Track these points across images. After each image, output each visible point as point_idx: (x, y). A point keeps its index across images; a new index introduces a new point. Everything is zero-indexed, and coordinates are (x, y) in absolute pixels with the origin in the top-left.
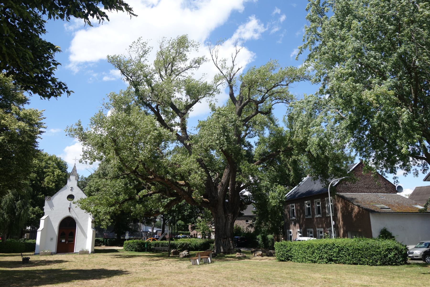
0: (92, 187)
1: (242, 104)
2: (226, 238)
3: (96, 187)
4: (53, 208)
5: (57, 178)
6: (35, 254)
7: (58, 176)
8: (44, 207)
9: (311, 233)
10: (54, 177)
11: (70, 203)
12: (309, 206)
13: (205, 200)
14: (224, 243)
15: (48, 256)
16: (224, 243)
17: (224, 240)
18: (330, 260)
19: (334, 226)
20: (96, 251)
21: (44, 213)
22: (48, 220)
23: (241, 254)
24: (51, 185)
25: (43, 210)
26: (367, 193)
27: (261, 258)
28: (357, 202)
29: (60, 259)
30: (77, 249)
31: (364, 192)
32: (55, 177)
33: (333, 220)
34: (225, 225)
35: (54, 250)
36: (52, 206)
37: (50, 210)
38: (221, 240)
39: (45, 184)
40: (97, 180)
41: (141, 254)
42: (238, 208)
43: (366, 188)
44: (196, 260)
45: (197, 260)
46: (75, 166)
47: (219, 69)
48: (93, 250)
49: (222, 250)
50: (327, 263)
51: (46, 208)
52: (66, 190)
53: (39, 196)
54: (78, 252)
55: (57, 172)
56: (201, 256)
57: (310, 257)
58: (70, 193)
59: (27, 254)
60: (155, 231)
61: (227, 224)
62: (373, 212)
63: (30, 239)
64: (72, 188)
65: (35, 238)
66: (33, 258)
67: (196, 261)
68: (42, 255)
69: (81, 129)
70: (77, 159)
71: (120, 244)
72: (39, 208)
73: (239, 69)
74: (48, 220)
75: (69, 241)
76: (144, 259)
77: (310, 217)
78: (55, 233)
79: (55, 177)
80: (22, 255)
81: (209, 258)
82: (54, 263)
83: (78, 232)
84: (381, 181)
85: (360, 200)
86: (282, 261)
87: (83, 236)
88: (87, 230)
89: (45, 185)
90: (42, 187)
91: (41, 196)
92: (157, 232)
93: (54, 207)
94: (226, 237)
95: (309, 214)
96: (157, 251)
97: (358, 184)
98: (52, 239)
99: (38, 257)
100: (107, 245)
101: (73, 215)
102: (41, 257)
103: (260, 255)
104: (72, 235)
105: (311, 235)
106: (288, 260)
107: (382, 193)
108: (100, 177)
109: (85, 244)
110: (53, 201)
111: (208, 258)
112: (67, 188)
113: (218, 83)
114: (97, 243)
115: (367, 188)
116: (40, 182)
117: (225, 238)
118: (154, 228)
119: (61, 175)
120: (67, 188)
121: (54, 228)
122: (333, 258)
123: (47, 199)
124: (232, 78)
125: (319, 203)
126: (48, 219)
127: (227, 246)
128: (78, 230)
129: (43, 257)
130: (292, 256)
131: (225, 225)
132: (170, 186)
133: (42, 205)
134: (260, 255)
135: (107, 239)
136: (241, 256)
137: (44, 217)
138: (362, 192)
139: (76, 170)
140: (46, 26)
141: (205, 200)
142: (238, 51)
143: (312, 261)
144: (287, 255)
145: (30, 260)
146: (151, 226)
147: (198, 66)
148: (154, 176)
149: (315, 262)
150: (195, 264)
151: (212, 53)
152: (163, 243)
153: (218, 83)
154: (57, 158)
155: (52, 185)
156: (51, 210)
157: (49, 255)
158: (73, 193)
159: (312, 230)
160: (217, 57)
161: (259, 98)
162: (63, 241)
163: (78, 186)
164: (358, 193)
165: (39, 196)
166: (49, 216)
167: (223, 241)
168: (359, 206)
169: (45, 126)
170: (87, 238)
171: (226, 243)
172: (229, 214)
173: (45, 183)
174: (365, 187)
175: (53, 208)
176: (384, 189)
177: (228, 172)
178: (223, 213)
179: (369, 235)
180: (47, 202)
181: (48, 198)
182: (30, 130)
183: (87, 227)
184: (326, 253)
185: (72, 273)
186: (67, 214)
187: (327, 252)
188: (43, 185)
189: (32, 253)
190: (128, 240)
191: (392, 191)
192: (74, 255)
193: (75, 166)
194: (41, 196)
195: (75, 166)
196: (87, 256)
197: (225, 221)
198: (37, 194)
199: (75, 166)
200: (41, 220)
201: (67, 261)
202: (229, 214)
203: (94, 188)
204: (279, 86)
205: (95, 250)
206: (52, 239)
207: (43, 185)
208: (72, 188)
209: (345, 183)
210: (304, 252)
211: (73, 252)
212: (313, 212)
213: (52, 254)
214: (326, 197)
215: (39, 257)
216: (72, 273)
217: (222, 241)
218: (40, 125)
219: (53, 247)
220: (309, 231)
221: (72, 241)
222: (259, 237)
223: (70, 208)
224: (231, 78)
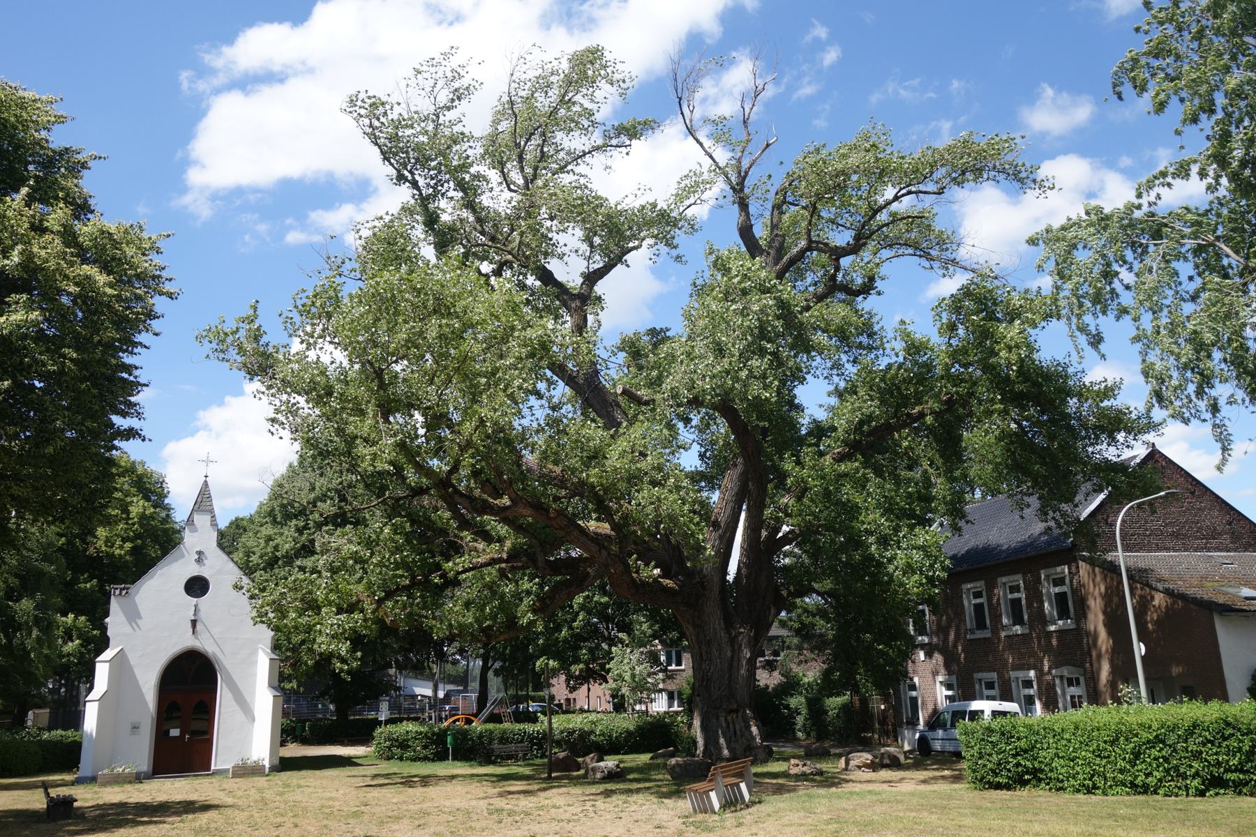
0: (254, 554)
1: (785, 260)
2: (736, 711)
3: (266, 554)
4: (139, 622)
5: (141, 525)
6: (78, 782)
7: (143, 517)
8: (107, 620)
9: (990, 686)
10: (127, 524)
11: (196, 606)
12: (978, 601)
13: (667, 582)
14: (728, 725)
15: (128, 787)
16: (728, 725)
17: (729, 718)
18: (1215, 783)
19: (1143, 658)
20: (285, 765)
21: (108, 639)
22: (121, 666)
23: (804, 765)
24: (121, 547)
25: (104, 628)
26: (1176, 551)
27: (869, 775)
28: (1159, 580)
29: (162, 798)
30: (222, 758)
31: (1168, 549)
32: (134, 524)
33: (1140, 640)
34: (731, 666)
35: (144, 764)
36: (133, 616)
37: (127, 629)
38: (718, 718)
39: (97, 545)
40: (268, 530)
41: (441, 769)
42: (769, 609)
43: (1172, 534)
44: (707, 793)
45: (713, 795)
46: (206, 484)
47: (701, 144)
48: (277, 762)
49: (726, 752)
50: (1202, 794)
51: (116, 622)
52: (181, 561)
53: (82, 586)
54: (227, 770)
55: (138, 507)
56: (724, 777)
57: (1121, 771)
58: (193, 570)
59: (62, 785)
60: (441, 694)
61: (735, 664)
62: (1226, 610)
63: (50, 729)
64: (200, 553)
65: (75, 720)
66: (86, 797)
67: (709, 798)
68: (104, 784)
69: (256, 336)
70: (204, 464)
71: (362, 734)
72: (88, 620)
73: (768, 145)
74: (121, 666)
75: (194, 733)
76: (478, 789)
77: (987, 634)
78: (145, 703)
79: (134, 524)
80: (45, 786)
81: (743, 786)
82: (178, 813)
83: (224, 698)
84: (1216, 513)
85: (1165, 573)
86: (998, 786)
87: (240, 716)
88: (253, 694)
89: (98, 551)
90: (90, 557)
91: (88, 586)
92: (448, 695)
93: (140, 618)
94: (735, 706)
95: (981, 625)
96: (488, 760)
97: (1146, 522)
98: (135, 728)
99: (96, 793)
100: (305, 741)
101: (206, 645)
102: (103, 789)
103: (867, 766)
104: (206, 709)
105: (987, 692)
106: (1024, 783)
107: (1221, 550)
108: (275, 522)
109: (247, 740)
110: (137, 599)
111: (737, 785)
112: (183, 556)
113: (687, 202)
114: (288, 732)
115: (1175, 535)
116: (84, 541)
117: (732, 711)
118: (441, 686)
119: (152, 517)
120: (183, 556)
121: (144, 691)
122: (1229, 776)
123: (117, 592)
124: (747, 173)
125: (978, 595)
126: (120, 663)
127: (742, 736)
128: (223, 696)
129: (109, 789)
130: (1042, 771)
131: (731, 666)
132: (563, 533)
133: (97, 611)
134: (867, 766)
135: (304, 721)
136: (807, 769)
137: (108, 654)
138: (1159, 549)
139: (210, 497)
140: (50, 139)
141: (667, 582)
142: (760, 87)
143: (1133, 785)
144: (1018, 765)
145: (76, 804)
146: (431, 677)
147: (628, 142)
148: (511, 499)
149: (1145, 789)
150: (707, 809)
151: (679, 91)
152: (505, 732)
153: (687, 202)
154: (134, 462)
155: (121, 550)
156: (131, 630)
157: (130, 782)
158: (205, 572)
159: (994, 676)
160: (691, 108)
161: (841, 238)
162: (175, 732)
163: (221, 546)
164: (1149, 551)
165: (82, 586)
166: (125, 650)
167: (726, 719)
168: (1168, 592)
169: (168, 287)
170: (254, 720)
171: (737, 728)
172: (742, 630)
173: (100, 543)
174: (1167, 532)
175: (139, 622)
176: (1226, 540)
177: (736, 489)
178: (723, 626)
179: (1214, 688)
180: (118, 603)
181: (121, 590)
182: (119, 298)
183: (254, 685)
184: (1197, 755)
185: (146, 819)
186: (184, 641)
187: (1201, 752)
188: (91, 550)
189: (68, 777)
190: (388, 722)
191: (1250, 545)
192: (214, 780)
193: (206, 484)
194: (88, 586)
195: (206, 481)
196: (261, 781)
197: (729, 654)
198: (75, 581)
199: (206, 481)
200: (97, 665)
201: (206, 808)
202: (742, 630)
203: (261, 557)
204: (914, 196)
205: (282, 759)
206: (135, 728)
207: (91, 550)
208: (200, 553)
209: (1106, 521)
210: (1099, 756)
211: (209, 769)
212: (997, 618)
213: (138, 778)
214: (1045, 567)
215: (96, 789)
216: (146, 819)
217: (722, 719)
218: (152, 281)
219: (141, 753)
220: (980, 680)
221: (205, 733)
222: (796, 701)
223: (194, 623)
224: (743, 174)
